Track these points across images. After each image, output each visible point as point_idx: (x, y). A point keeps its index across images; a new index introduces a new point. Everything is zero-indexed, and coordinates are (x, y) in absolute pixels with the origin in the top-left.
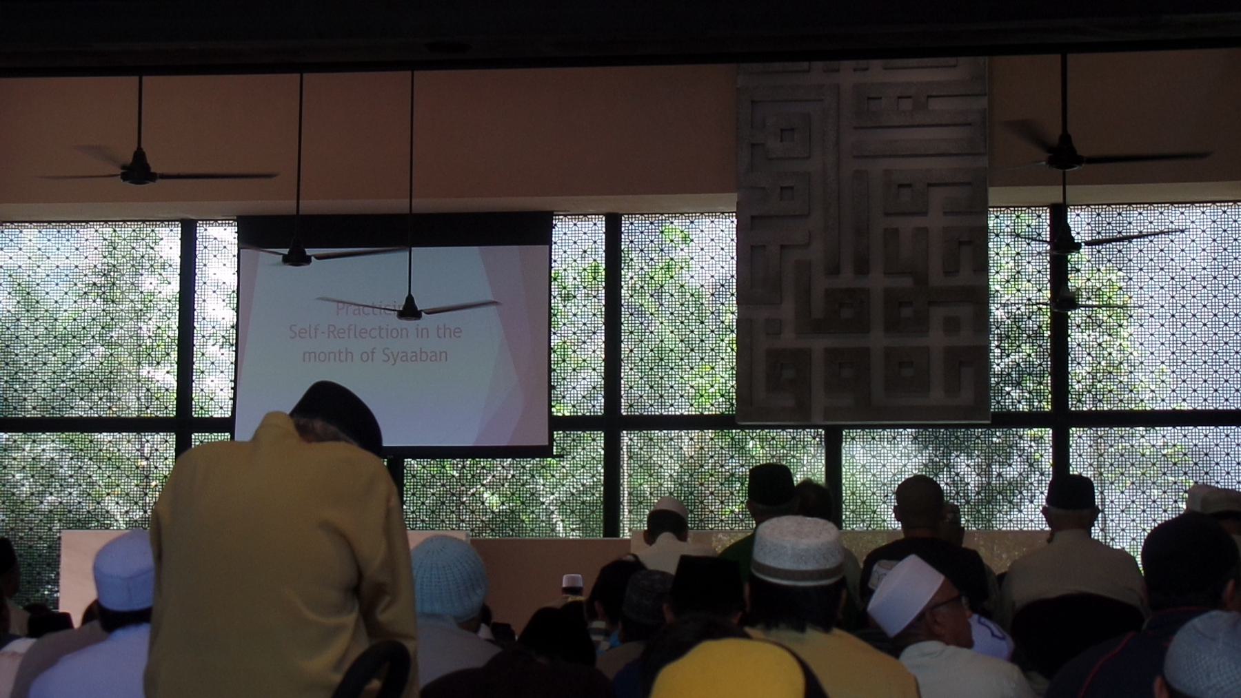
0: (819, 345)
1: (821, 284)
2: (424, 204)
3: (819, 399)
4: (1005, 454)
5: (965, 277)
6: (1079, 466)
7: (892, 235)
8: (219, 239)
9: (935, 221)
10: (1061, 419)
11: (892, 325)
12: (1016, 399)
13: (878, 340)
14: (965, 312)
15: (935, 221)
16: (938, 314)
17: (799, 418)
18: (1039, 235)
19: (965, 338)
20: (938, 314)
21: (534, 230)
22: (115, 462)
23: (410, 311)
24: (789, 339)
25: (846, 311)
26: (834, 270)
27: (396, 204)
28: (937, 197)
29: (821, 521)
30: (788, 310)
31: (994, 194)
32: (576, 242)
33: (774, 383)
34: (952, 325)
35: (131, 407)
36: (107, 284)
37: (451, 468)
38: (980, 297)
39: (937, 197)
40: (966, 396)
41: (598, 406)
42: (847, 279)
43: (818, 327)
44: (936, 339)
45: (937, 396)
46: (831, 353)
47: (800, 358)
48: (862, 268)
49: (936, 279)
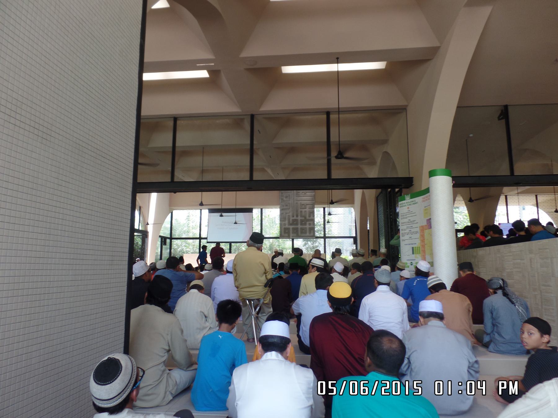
0: (291, 227)
1: (291, 218)
2: (238, 207)
3: (291, 235)
4: (316, 241)
5: (311, 218)
6: (350, 215)
7: (301, 212)
8: (205, 212)
9: (307, 210)
10: (325, 237)
11: (301, 224)
12: (317, 234)
13: (299, 226)
14: (311, 222)
15: (307, 210)
16: (308, 223)
17: (288, 237)
18: (328, 222)
19: (311, 226)
20: (308, 223)
21: (250, 210)
22: (189, 244)
23: (236, 223)
24: (287, 226)
25: (295, 222)
26: (293, 216)
27: (234, 207)
28: (308, 206)
29: (159, 309)
30: (287, 222)
31: (315, 206)
32: (256, 212)
33: (285, 233)
34: (310, 224)
35: (191, 236)
36: (188, 218)
37: (238, 244)
38: (313, 220)
39: (308, 206)
40: (312, 234)
41: (173, 237)
42: (295, 218)
43: (291, 225)
44: (308, 226)
45: (308, 234)
46: (293, 228)
47: (288, 229)
48: (297, 216)
49: (308, 218)
